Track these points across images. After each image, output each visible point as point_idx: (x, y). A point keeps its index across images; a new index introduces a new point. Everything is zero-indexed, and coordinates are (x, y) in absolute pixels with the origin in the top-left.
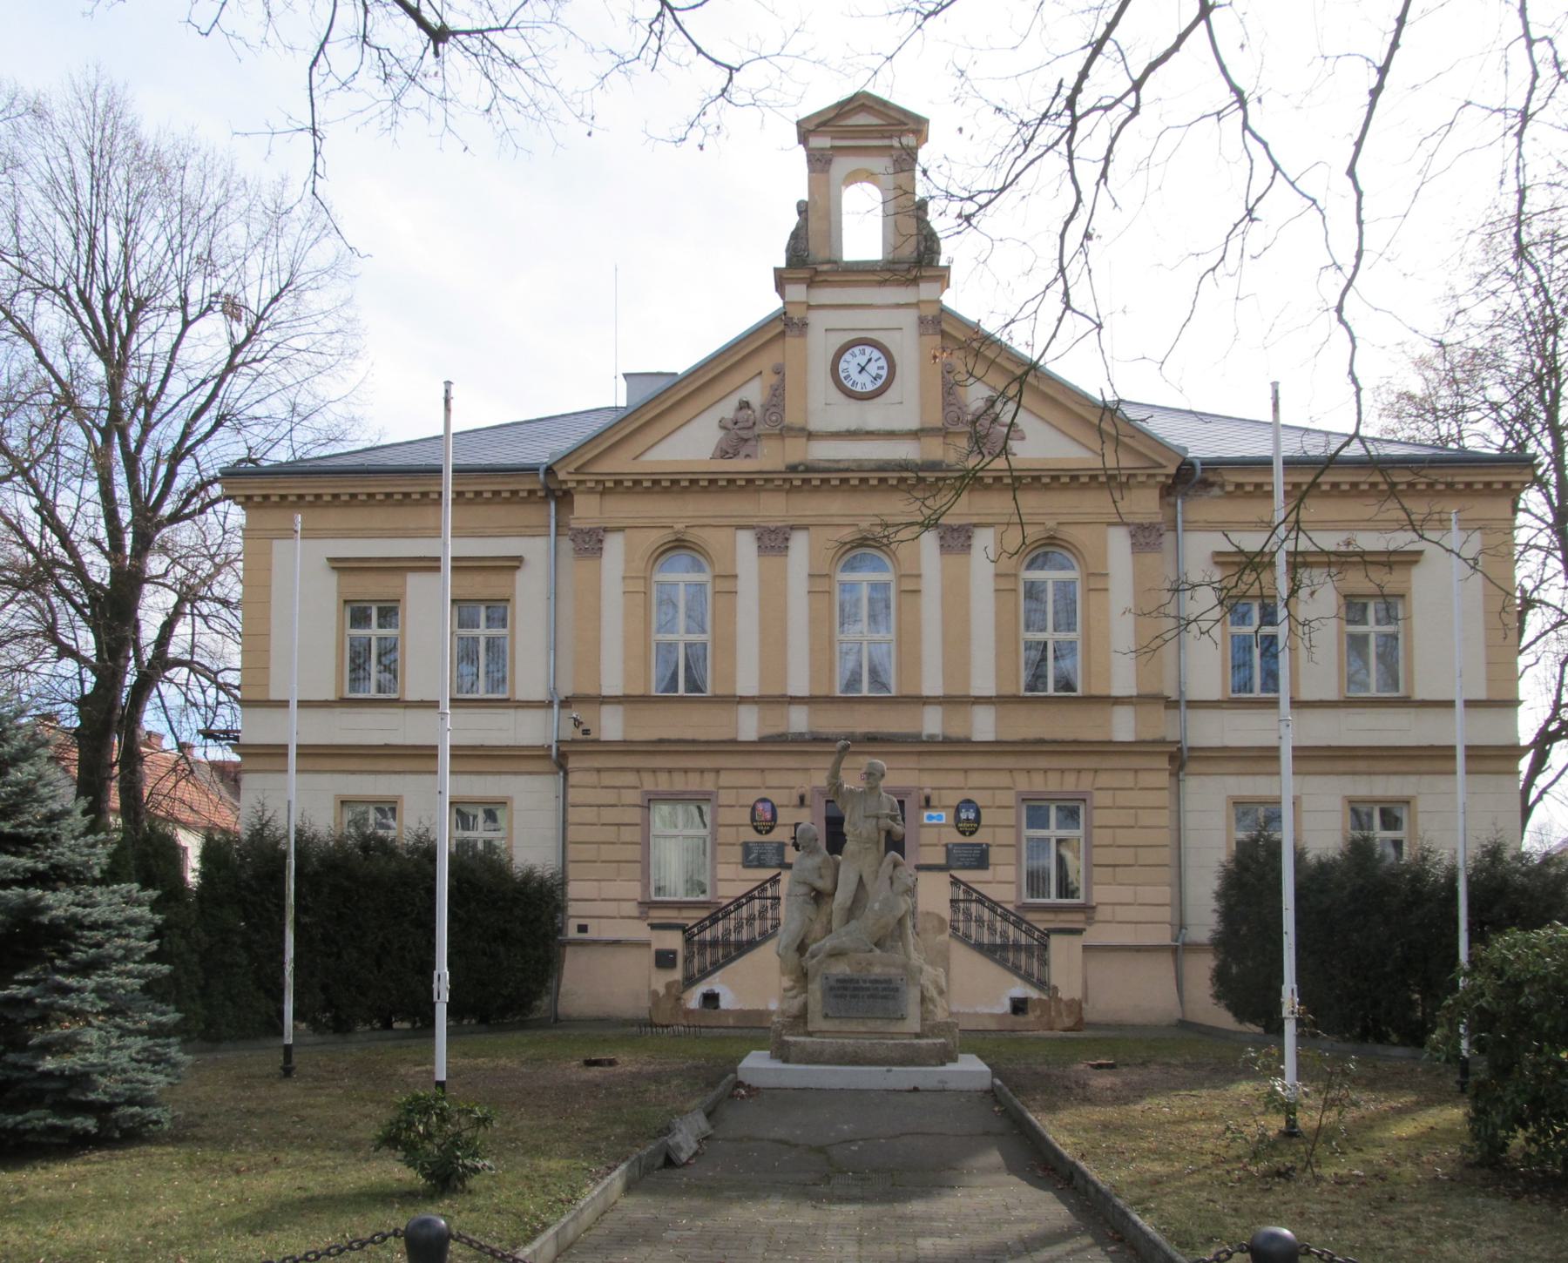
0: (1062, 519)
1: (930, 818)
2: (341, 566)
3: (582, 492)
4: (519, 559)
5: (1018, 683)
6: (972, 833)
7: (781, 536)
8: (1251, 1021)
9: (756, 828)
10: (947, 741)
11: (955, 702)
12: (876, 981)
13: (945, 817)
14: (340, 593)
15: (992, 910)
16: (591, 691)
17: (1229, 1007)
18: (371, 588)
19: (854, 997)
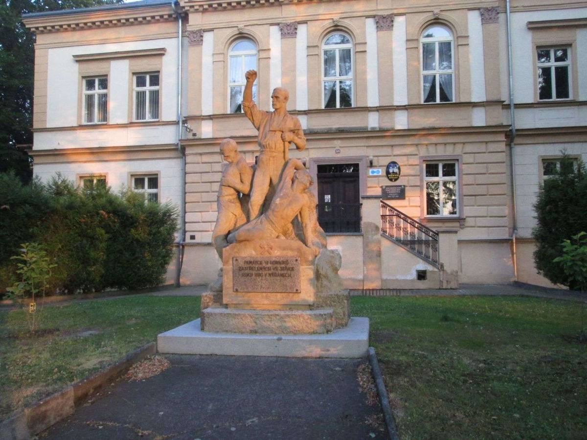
0: (443, 8)
1: (373, 172)
2: (80, 60)
3: (193, 12)
4: (163, 49)
5: (420, 98)
6: (396, 180)
7: (293, 28)
8: (562, 283)
9: (388, 177)
10: (382, 130)
11: (385, 109)
12: (276, 262)
13: (381, 172)
14: (79, 73)
15: (405, 220)
16: (197, 114)
17: (546, 275)
18: (94, 69)
19: (259, 275)
